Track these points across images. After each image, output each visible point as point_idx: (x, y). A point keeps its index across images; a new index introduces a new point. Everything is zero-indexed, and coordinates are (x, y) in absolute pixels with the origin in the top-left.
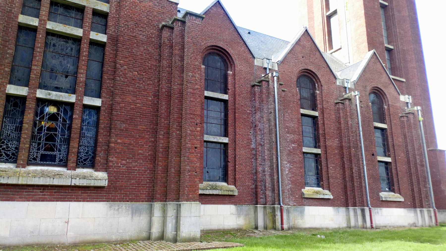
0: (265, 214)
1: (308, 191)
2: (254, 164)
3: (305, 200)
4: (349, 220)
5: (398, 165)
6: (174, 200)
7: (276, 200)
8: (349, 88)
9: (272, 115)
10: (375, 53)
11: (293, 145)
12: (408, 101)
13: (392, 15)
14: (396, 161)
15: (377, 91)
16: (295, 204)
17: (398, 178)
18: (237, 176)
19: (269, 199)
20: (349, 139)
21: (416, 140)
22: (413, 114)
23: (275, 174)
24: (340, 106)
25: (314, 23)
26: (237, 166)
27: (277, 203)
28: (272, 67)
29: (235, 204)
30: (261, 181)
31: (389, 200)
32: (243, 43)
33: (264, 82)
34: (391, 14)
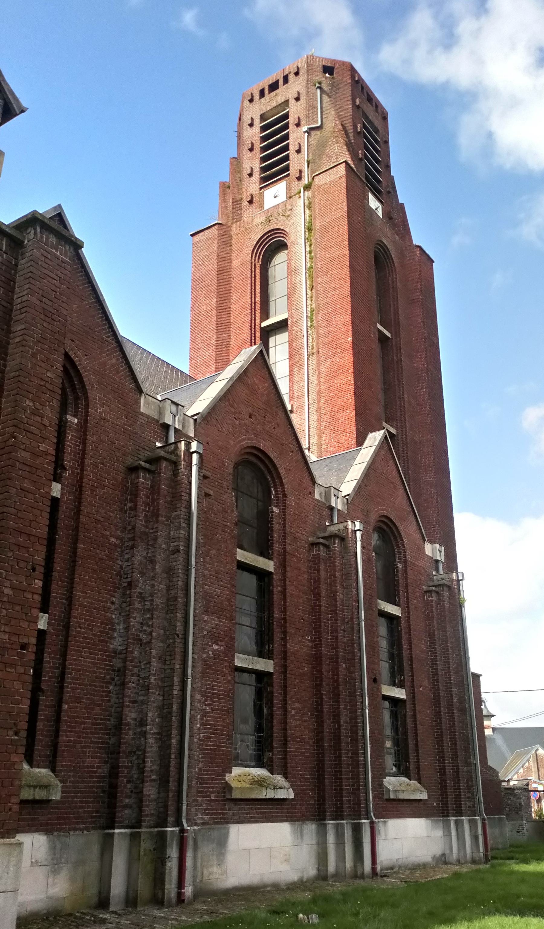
0: (132, 859)
1: (242, 776)
2: (113, 700)
3: (232, 805)
4: (322, 857)
5: (418, 708)
6: (162, 864)
7: (169, 811)
8: (338, 510)
9: (181, 557)
10: (386, 437)
11: (215, 647)
12: (439, 558)
13: (397, 362)
14: (414, 697)
15: (385, 527)
16: (207, 818)
17: (417, 741)
18: (63, 738)
19: (150, 809)
20: (337, 637)
21: (452, 648)
22: (449, 587)
23: (174, 732)
24: (321, 553)
25: (229, 337)
26: (65, 707)
27: (171, 819)
28: (183, 426)
29: (46, 834)
30: (130, 752)
31: (402, 796)
32: (115, 345)
33: (164, 464)
34: (395, 358)
